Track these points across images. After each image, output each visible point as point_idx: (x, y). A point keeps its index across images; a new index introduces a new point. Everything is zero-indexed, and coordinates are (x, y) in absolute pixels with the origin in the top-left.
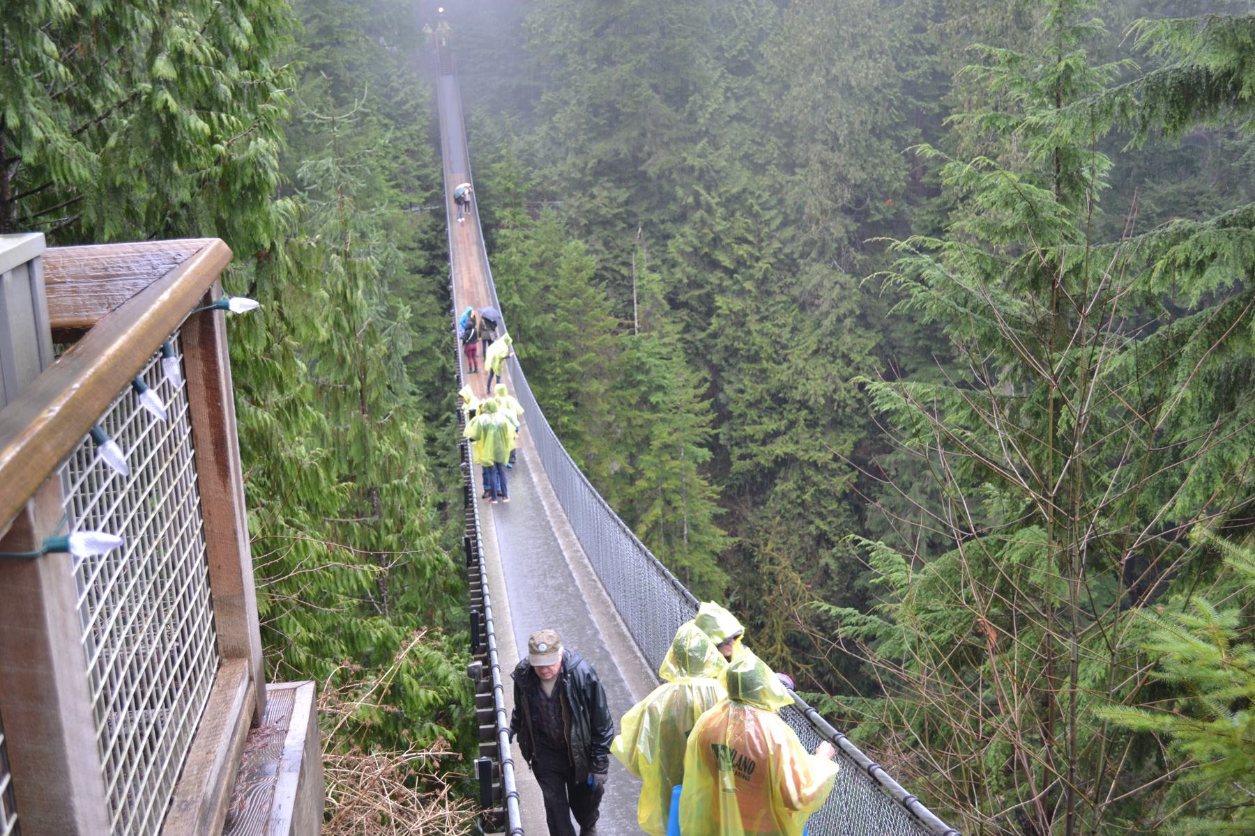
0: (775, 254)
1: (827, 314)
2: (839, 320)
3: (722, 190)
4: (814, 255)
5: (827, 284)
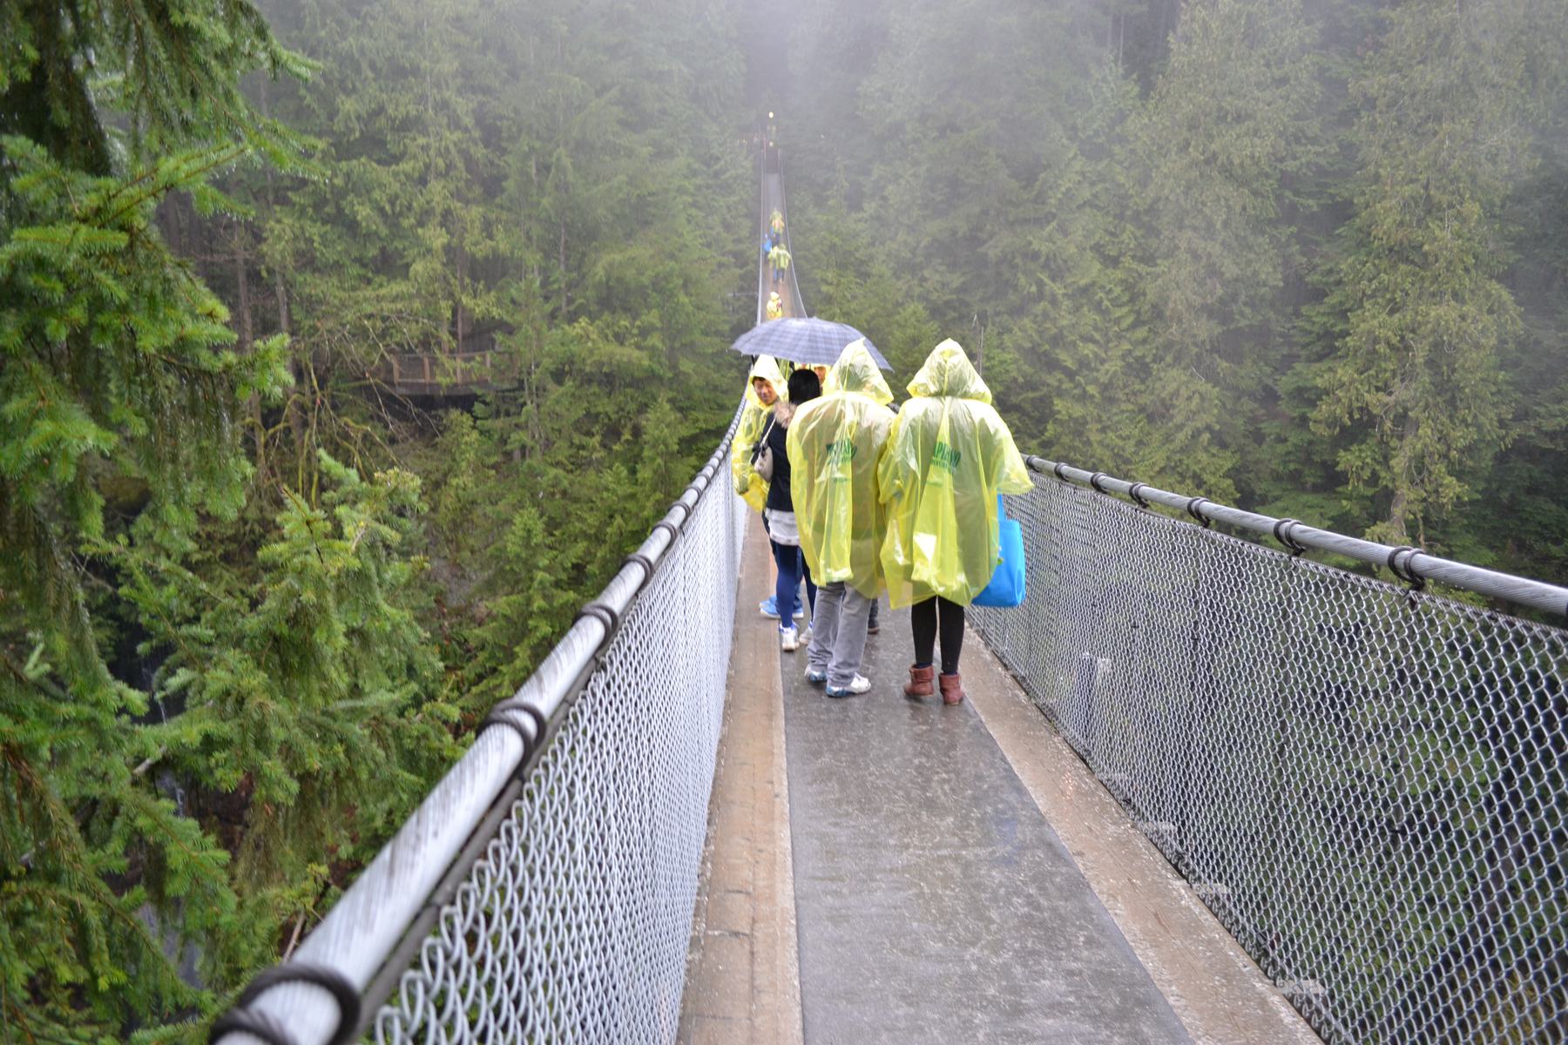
0: (1123, 357)
1: (1180, 427)
2: (1196, 435)
3: (1070, 280)
4: (1169, 359)
5: (1184, 392)
